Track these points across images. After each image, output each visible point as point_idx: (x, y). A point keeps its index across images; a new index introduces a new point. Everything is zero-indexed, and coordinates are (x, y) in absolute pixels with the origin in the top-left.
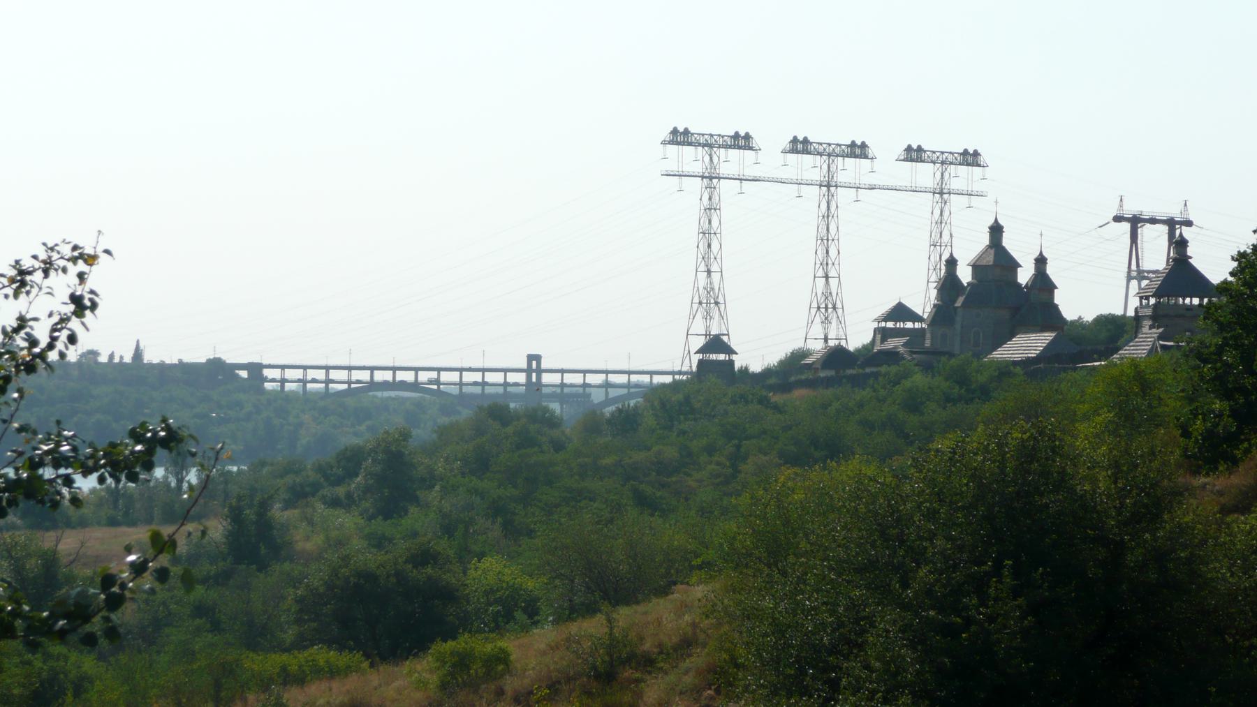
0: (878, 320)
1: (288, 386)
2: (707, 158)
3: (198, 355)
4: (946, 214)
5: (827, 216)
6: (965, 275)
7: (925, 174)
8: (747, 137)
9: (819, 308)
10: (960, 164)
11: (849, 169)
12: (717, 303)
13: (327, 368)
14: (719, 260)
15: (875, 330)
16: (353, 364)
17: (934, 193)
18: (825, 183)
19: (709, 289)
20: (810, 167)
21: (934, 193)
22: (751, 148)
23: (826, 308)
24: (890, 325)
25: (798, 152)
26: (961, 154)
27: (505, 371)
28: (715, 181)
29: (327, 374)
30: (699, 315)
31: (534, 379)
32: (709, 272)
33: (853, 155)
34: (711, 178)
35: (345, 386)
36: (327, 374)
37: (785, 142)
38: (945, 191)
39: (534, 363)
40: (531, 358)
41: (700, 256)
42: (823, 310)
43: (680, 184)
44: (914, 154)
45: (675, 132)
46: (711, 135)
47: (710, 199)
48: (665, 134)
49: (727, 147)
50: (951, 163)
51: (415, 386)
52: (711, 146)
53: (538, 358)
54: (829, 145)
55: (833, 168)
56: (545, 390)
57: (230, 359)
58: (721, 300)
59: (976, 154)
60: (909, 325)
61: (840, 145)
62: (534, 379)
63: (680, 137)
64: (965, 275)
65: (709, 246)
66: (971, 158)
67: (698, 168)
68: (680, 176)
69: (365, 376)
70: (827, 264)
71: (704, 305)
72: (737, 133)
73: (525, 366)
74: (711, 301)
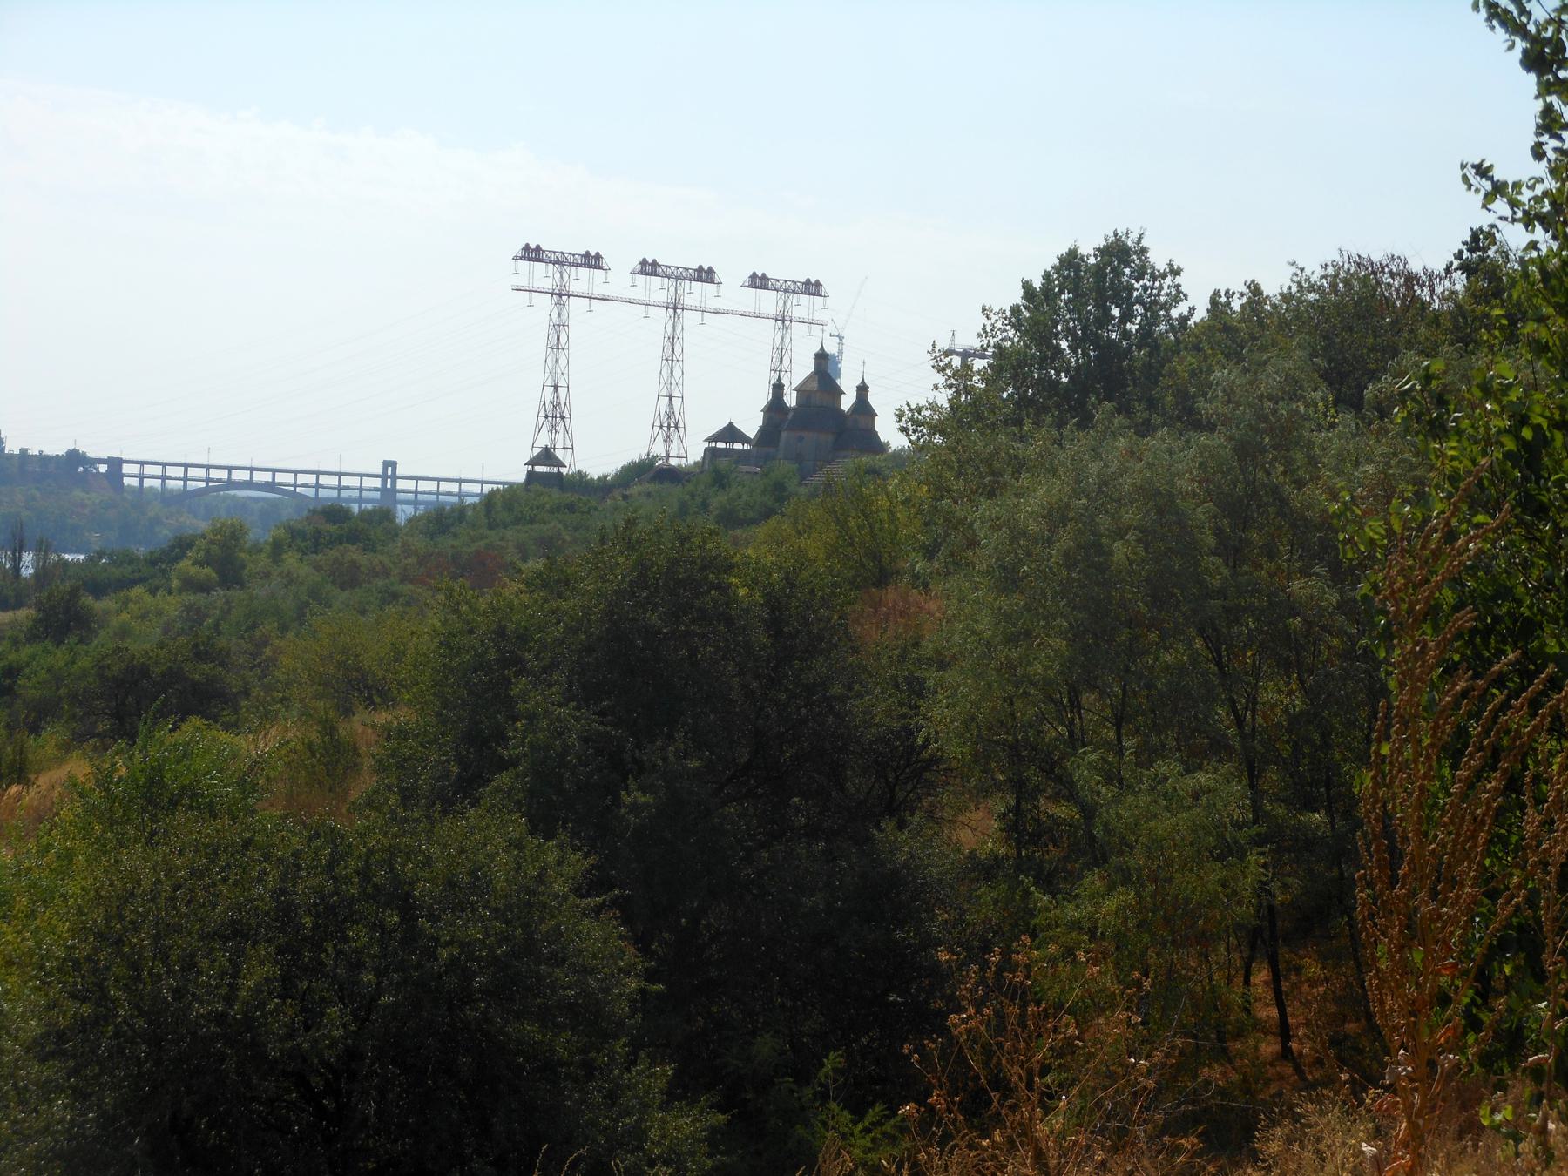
0: (709, 440)
1: (147, 483)
2: (557, 276)
3: (56, 447)
4: (787, 340)
5: (558, 326)
6: (791, 399)
7: (769, 301)
8: (598, 257)
9: (661, 427)
10: (802, 293)
11: (695, 293)
12: (562, 418)
13: (318, 473)
14: (566, 376)
15: (706, 450)
16: (343, 470)
17: (776, 320)
18: (672, 305)
19: (556, 404)
20: (657, 289)
21: (776, 320)
22: (601, 268)
23: (669, 427)
24: (721, 445)
25: (647, 274)
26: (803, 283)
27: (362, 476)
28: (564, 298)
29: (208, 473)
30: (545, 430)
31: (389, 486)
32: (556, 387)
33: (586, 265)
34: (560, 295)
35: (203, 485)
36: (186, 471)
37: (634, 263)
38: (787, 318)
39: (390, 469)
40: (386, 464)
41: (547, 371)
42: (665, 429)
43: (531, 299)
44: (758, 282)
45: (527, 248)
46: (563, 253)
47: (559, 315)
48: (517, 249)
49: (577, 265)
50: (794, 292)
51: (271, 486)
52: (561, 264)
53: (393, 464)
54: (678, 268)
55: (680, 291)
56: (400, 496)
57: (92, 453)
58: (566, 414)
59: (818, 284)
60: (738, 446)
61: (688, 269)
62: (389, 486)
63: (532, 254)
64: (791, 399)
65: (557, 361)
66: (812, 288)
67: (548, 285)
68: (530, 291)
69: (223, 475)
70: (671, 384)
71: (550, 419)
72: (587, 252)
73: (380, 472)
74: (556, 414)
